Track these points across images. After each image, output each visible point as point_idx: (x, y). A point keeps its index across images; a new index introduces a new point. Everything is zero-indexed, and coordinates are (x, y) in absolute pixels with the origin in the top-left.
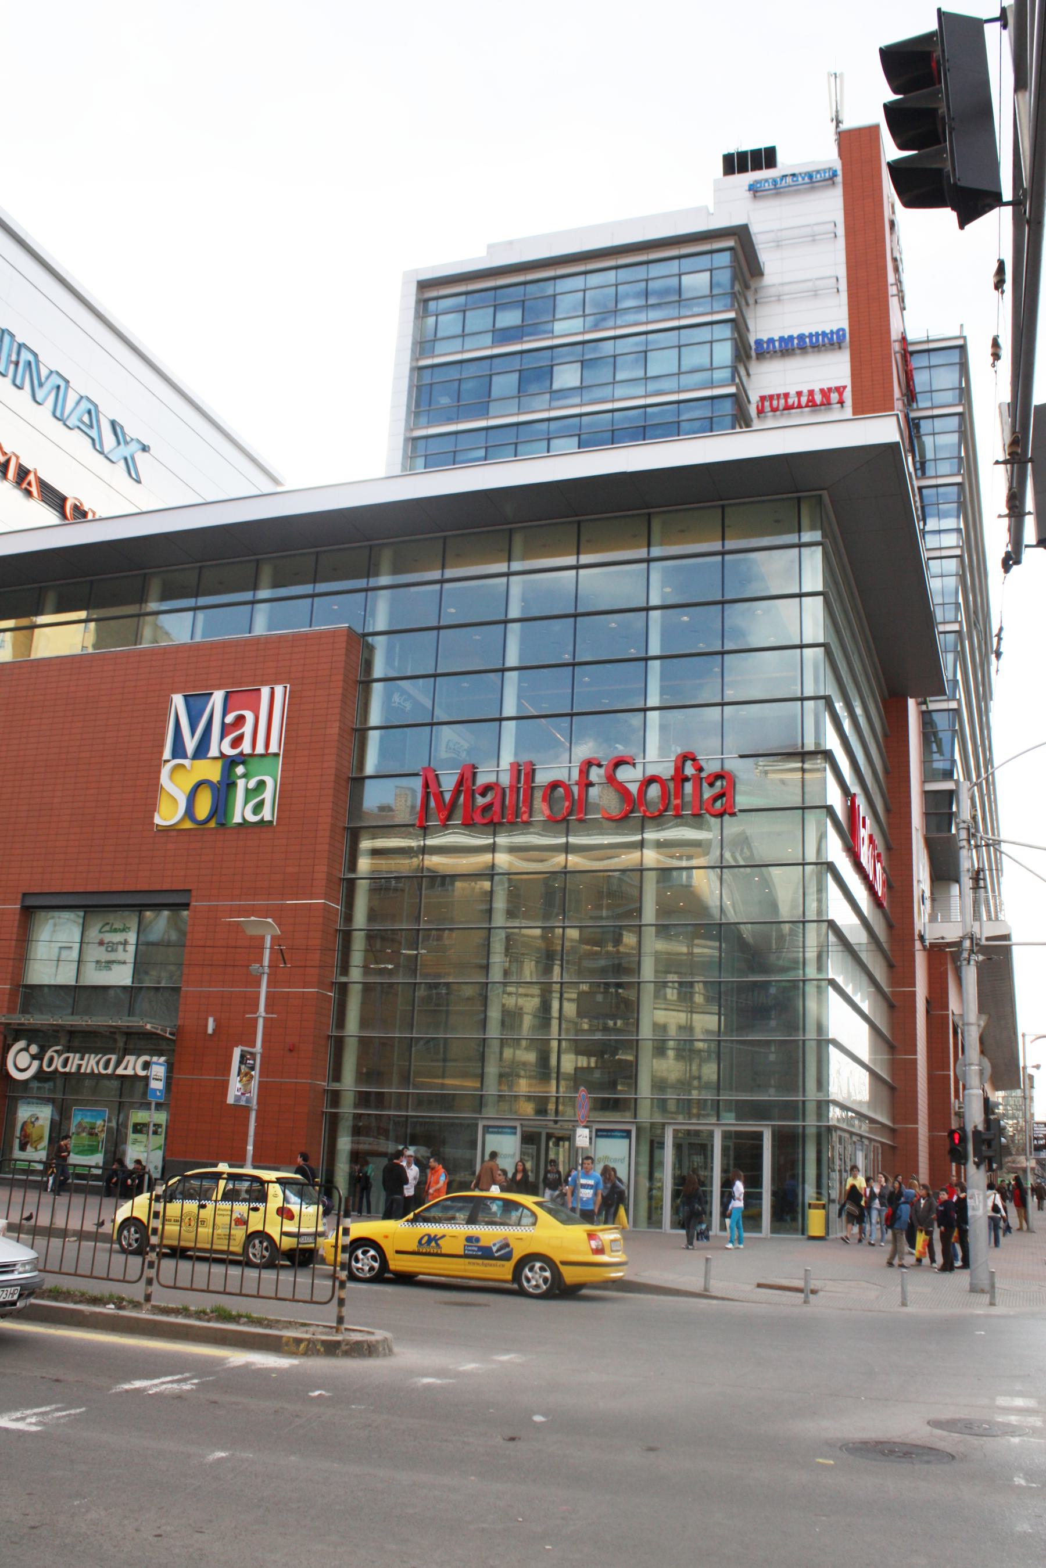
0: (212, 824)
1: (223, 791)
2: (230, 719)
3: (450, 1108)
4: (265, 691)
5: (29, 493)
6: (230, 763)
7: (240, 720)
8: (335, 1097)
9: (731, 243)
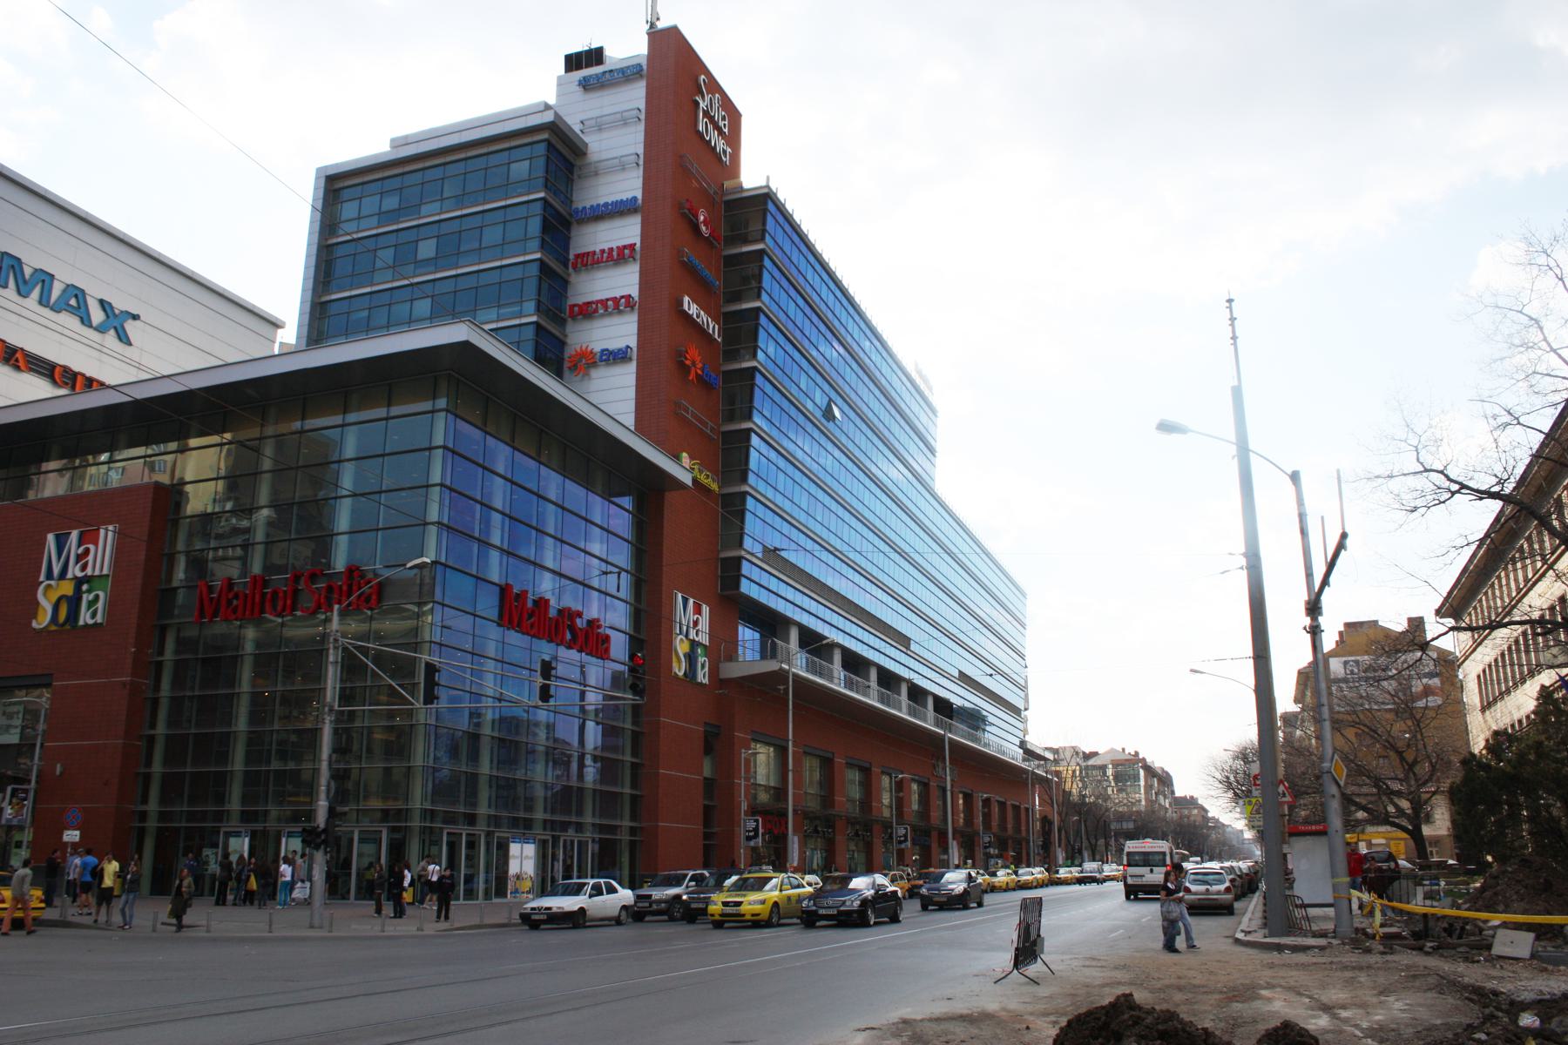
0: (67, 627)
1: (74, 602)
2: (81, 550)
3: (1051, 823)
4: (102, 532)
5: (18, 368)
6: (79, 582)
7: (87, 551)
8: (143, 816)
9: (545, 136)
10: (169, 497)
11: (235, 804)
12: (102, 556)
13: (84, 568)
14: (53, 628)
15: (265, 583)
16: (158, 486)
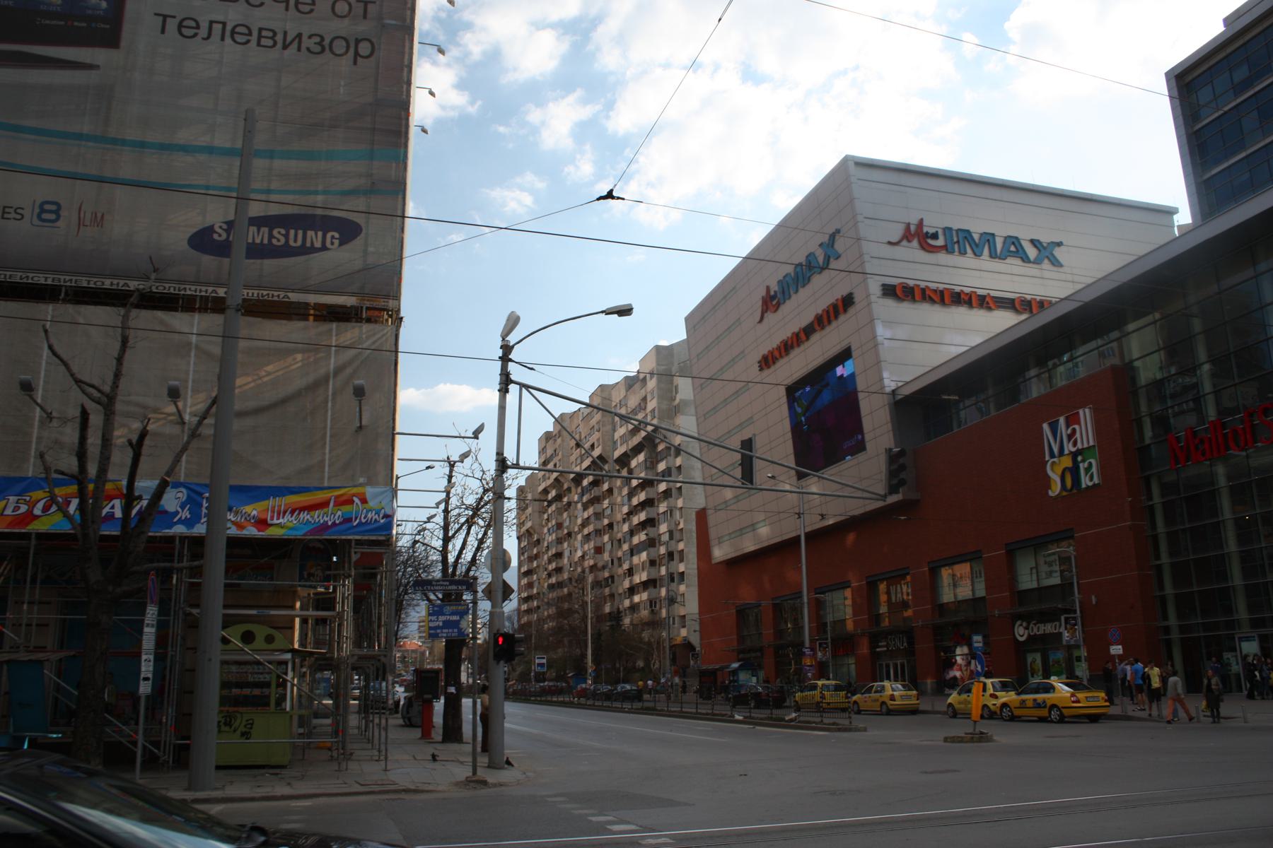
1: (1074, 470)
4: (1081, 412)
5: (989, 309)
6: (1074, 455)
7: (1074, 431)
10: (1124, 374)
11: (1242, 613)
12: (1086, 433)
13: (1075, 444)
14: (1064, 493)
15: (1224, 426)
16: (1114, 369)
